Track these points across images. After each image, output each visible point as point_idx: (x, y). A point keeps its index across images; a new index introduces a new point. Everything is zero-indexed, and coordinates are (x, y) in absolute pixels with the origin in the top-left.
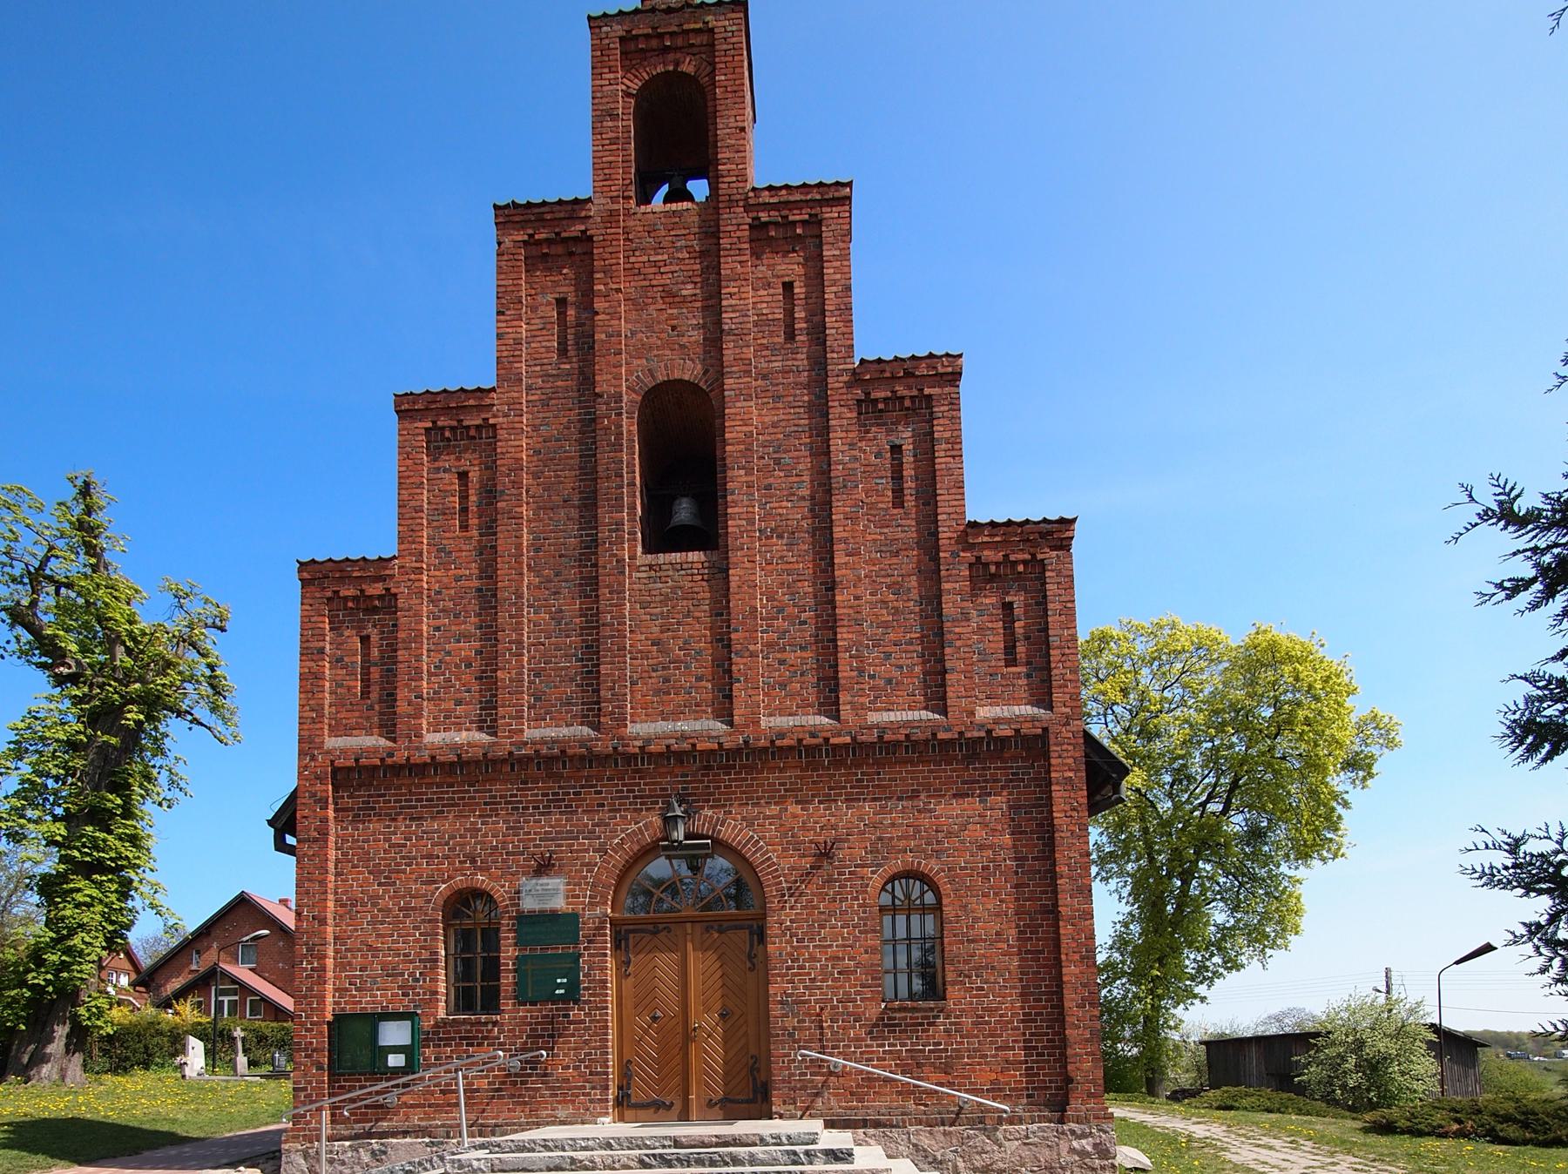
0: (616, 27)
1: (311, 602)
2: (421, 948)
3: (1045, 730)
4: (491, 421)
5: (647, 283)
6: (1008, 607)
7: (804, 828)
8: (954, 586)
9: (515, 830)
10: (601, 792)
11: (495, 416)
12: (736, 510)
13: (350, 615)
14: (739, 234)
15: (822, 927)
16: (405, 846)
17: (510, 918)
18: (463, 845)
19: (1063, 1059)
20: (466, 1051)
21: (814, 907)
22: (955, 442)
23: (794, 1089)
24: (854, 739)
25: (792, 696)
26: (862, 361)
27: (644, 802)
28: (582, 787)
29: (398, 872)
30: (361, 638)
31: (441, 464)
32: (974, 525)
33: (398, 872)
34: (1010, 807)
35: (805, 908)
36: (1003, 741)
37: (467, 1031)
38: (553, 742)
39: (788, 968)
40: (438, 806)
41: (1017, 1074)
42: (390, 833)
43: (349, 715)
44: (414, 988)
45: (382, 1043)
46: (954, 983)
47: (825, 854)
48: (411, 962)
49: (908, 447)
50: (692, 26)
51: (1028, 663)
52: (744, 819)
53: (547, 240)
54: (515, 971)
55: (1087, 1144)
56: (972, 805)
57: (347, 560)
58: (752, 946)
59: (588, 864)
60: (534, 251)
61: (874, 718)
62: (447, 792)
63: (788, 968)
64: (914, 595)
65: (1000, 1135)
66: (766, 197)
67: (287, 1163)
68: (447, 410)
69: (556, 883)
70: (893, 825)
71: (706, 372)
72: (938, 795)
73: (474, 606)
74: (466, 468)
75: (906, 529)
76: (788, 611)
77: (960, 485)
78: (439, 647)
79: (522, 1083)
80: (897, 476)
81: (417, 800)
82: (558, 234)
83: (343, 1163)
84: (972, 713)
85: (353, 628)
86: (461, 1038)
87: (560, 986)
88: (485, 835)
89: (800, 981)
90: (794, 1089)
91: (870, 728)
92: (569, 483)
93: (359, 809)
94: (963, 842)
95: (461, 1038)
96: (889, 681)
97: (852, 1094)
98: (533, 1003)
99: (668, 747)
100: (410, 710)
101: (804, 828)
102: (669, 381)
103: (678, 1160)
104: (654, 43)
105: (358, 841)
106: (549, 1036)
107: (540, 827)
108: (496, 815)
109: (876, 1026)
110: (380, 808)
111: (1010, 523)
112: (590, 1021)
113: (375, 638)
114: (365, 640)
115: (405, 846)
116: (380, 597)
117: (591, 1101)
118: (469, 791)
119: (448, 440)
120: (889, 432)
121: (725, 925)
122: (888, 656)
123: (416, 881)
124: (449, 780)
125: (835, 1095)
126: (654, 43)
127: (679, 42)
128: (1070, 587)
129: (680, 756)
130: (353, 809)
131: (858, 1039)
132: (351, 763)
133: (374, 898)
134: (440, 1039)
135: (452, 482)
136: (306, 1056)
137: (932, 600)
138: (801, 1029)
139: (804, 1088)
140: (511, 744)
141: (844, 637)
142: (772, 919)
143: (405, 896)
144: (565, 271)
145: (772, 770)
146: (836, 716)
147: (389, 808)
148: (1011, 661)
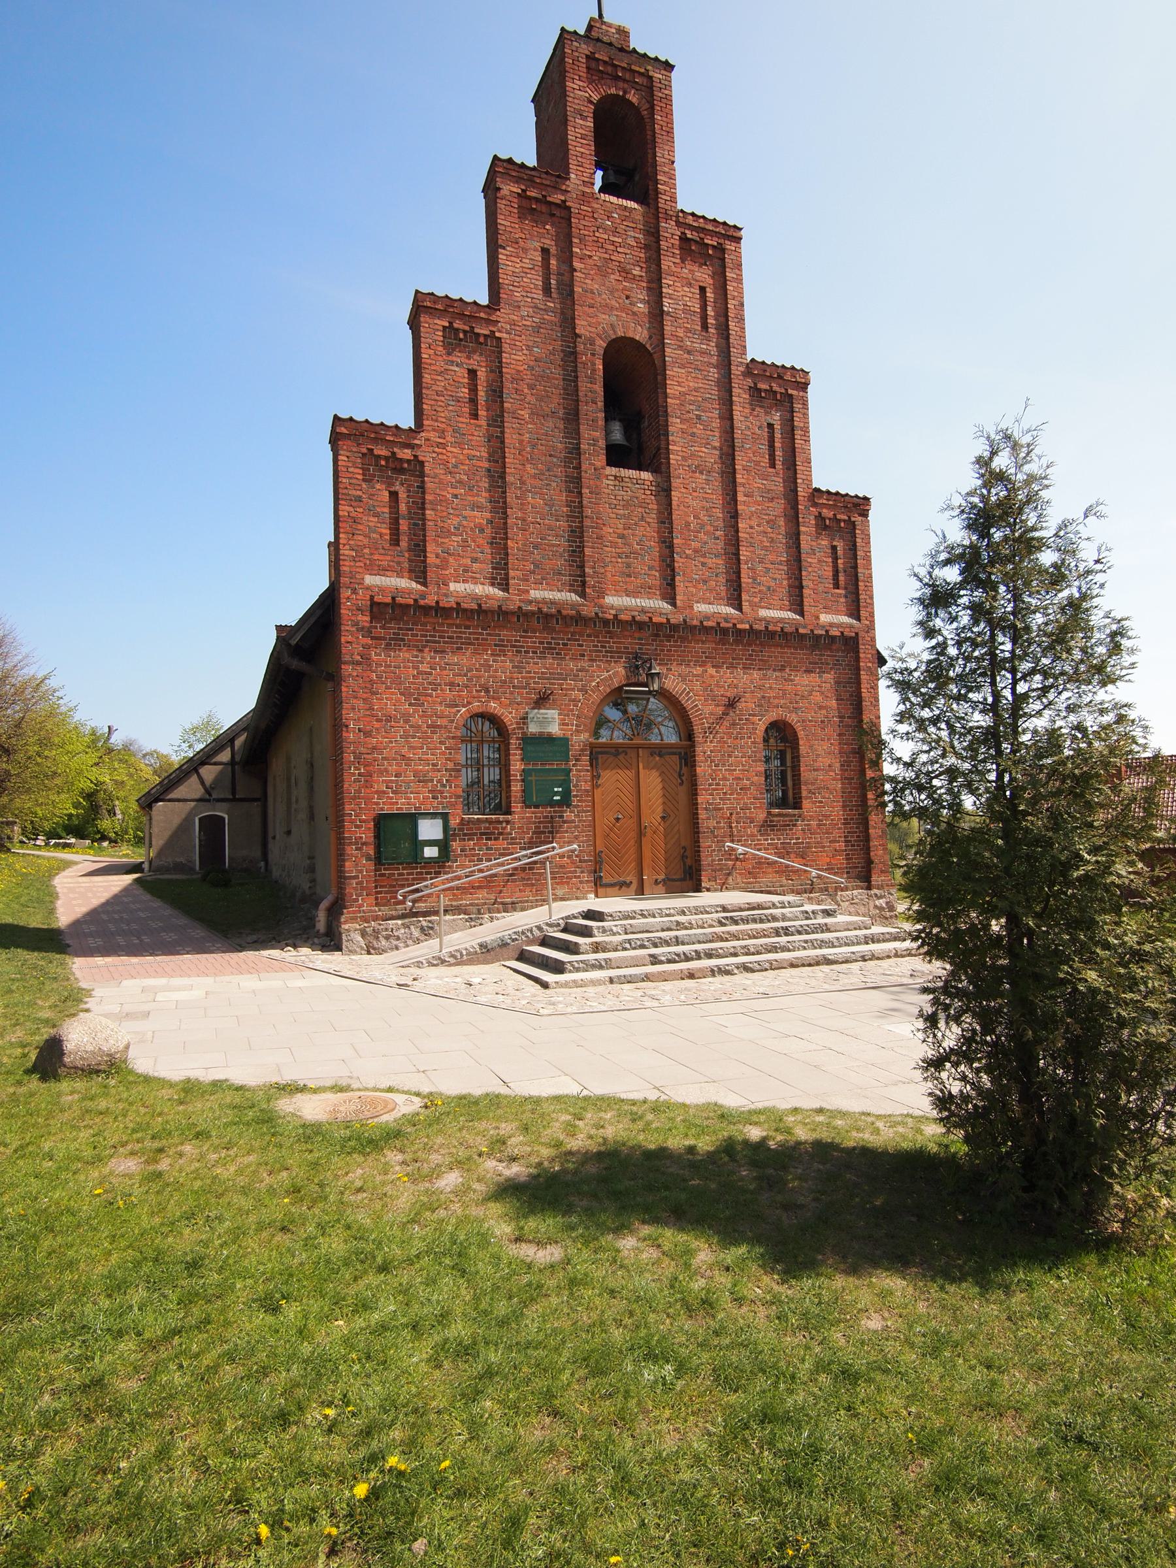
0: (584, 46)
2: (447, 759)
3: (857, 634)
4: (497, 334)
5: (607, 256)
6: (834, 548)
7: (717, 685)
8: (807, 528)
9: (519, 668)
12: (675, 448)
13: (380, 471)
15: (730, 756)
16: (431, 674)
17: (518, 739)
18: (479, 677)
19: (867, 850)
20: (486, 844)
22: (806, 430)
24: (751, 627)
26: (753, 360)
27: (613, 655)
28: (569, 640)
29: (427, 695)
31: (454, 359)
32: (817, 490)
33: (427, 695)
35: (719, 742)
36: (833, 638)
37: (486, 828)
41: (841, 858)
43: (381, 558)
44: (441, 792)
45: (420, 838)
47: (731, 704)
48: (439, 771)
49: (777, 427)
50: (637, 69)
51: (846, 588)
52: (680, 675)
54: (523, 781)
56: (814, 678)
64: (783, 530)
68: (461, 316)
69: (553, 714)
71: (650, 338)
72: (795, 669)
73: (485, 483)
75: (777, 484)
76: (708, 528)
78: (457, 512)
79: (530, 869)
80: (772, 446)
81: (440, 637)
82: (544, 196)
83: (398, 938)
84: (818, 618)
85: (384, 483)
86: (482, 834)
87: (557, 793)
88: (496, 671)
89: (718, 794)
92: (555, 402)
93: (391, 639)
94: (810, 703)
95: (482, 834)
96: (769, 588)
98: (536, 807)
99: (633, 617)
101: (717, 685)
102: (625, 338)
103: (742, 920)
104: (610, 69)
105: (390, 666)
106: (549, 832)
107: (539, 667)
109: (762, 826)
110: (409, 640)
111: (837, 494)
112: (580, 821)
113: (402, 495)
114: (394, 495)
115: (431, 674)
116: (409, 461)
117: (581, 882)
118: (482, 634)
119: (461, 340)
122: (768, 569)
123: (441, 703)
124: (468, 623)
125: (740, 874)
127: (628, 76)
129: (641, 626)
130: (385, 639)
131: (753, 835)
132: (388, 600)
133: (406, 718)
134: (465, 835)
135: (461, 374)
137: (795, 537)
138: (719, 828)
141: (744, 554)
142: (699, 749)
145: (697, 642)
147: (417, 641)
148: (837, 586)
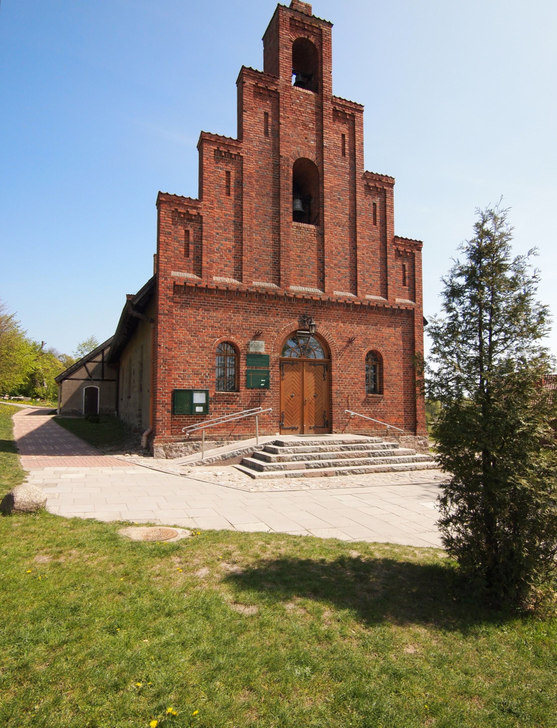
0: (289, 13)
1: (165, 211)
3: (414, 309)
4: (241, 154)
6: (404, 266)
7: (344, 332)
8: (391, 256)
9: (246, 320)
10: (277, 310)
11: (242, 153)
12: (327, 213)
14: (329, 111)
15: (349, 367)
16: (202, 321)
17: (244, 355)
20: (227, 406)
21: (347, 360)
22: (392, 207)
23: (339, 423)
24: (361, 303)
25: (342, 285)
26: (367, 171)
28: (271, 307)
29: (200, 332)
30: (185, 231)
32: (397, 237)
33: (200, 332)
34: (402, 332)
35: (344, 360)
36: (402, 310)
37: (227, 398)
38: (263, 288)
39: (338, 381)
40: (215, 306)
41: (402, 419)
42: (196, 315)
43: (180, 263)
44: (205, 380)
46: (386, 389)
47: (350, 341)
48: (205, 369)
49: (378, 205)
50: (315, 25)
51: (409, 286)
52: (325, 326)
53: (262, 88)
54: (246, 376)
55: (421, 442)
57: (182, 197)
58: (324, 372)
59: (272, 337)
60: (257, 90)
61: (368, 297)
62: (220, 301)
63: (338, 381)
64: (379, 256)
65: (400, 439)
66: (338, 101)
67: (157, 452)
69: (262, 343)
70: (370, 334)
71: (317, 159)
72: (382, 325)
74: (229, 170)
75: (377, 233)
77: (393, 222)
78: (218, 242)
82: (267, 87)
83: (181, 451)
84: (394, 300)
87: (262, 382)
88: (235, 321)
89: (342, 386)
90: (339, 423)
91: (366, 300)
92: (268, 189)
93: (183, 303)
94: (389, 342)
96: (371, 285)
97: (356, 425)
98: (252, 389)
99: (303, 297)
100: (208, 266)
101: (344, 332)
103: (352, 448)
105: (182, 317)
107: (256, 319)
108: (239, 313)
109: (364, 402)
110: (192, 304)
111: (406, 239)
112: (273, 397)
113: (191, 232)
114: (187, 232)
115: (202, 321)
117: (273, 427)
118: (228, 302)
119: (223, 156)
120: (373, 198)
121: (316, 363)
123: (207, 336)
124: (221, 297)
125: (352, 426)
126: (301, 25)
127: (310, 29)
128: (421, 264)
129: (307, 301)
131: (359, 407)
132: (183, 284)
134: (216, 401)
135: (222, 173)
136: (163, 407)
138: (342, 402)
139: (342, 423)
140: (248, 286)
141: (359, 267)
143: (202, 342)
144: (268, 102)
145: (334, 310)
146: (356, 294)
148: (404, 284)
